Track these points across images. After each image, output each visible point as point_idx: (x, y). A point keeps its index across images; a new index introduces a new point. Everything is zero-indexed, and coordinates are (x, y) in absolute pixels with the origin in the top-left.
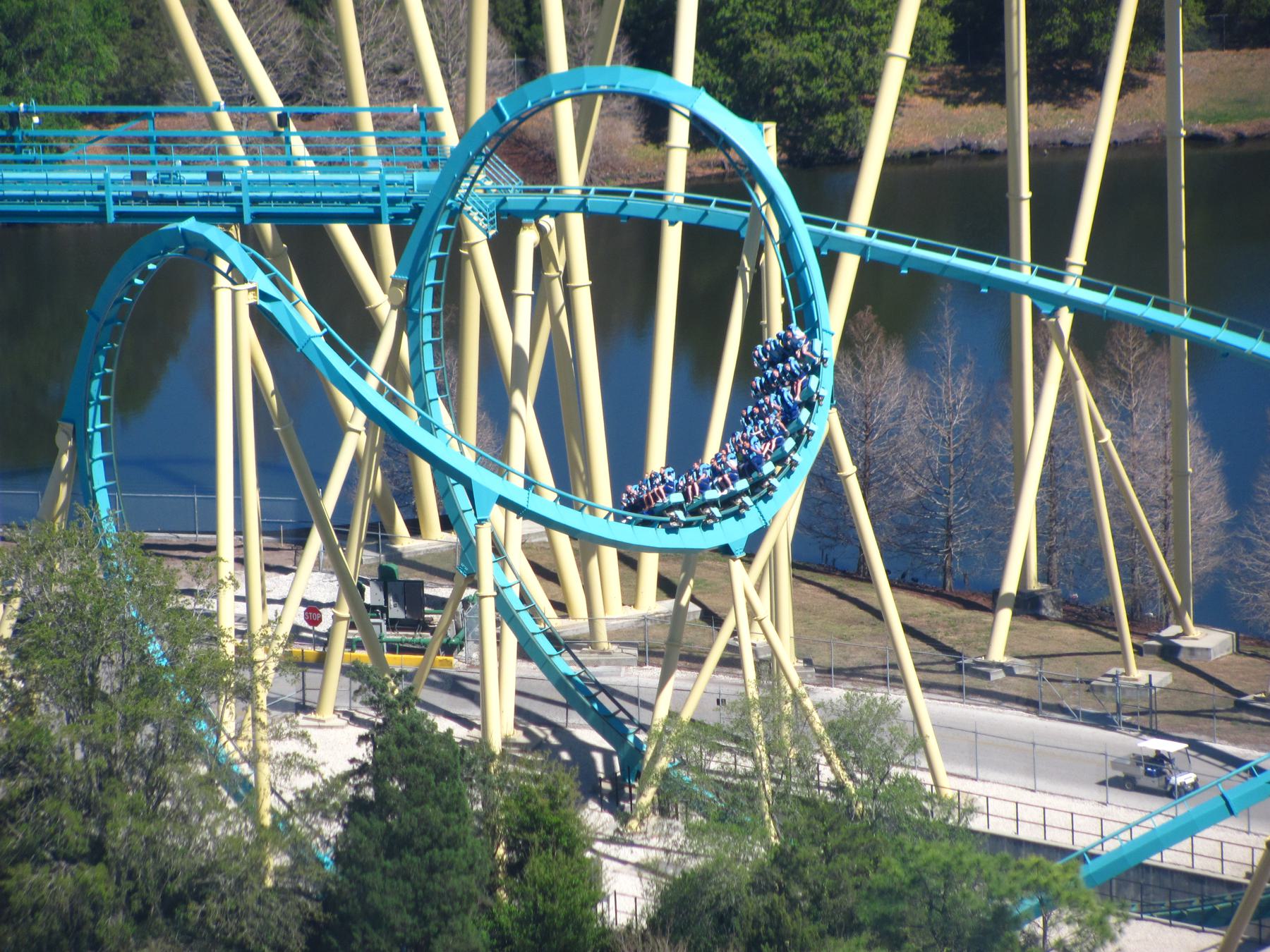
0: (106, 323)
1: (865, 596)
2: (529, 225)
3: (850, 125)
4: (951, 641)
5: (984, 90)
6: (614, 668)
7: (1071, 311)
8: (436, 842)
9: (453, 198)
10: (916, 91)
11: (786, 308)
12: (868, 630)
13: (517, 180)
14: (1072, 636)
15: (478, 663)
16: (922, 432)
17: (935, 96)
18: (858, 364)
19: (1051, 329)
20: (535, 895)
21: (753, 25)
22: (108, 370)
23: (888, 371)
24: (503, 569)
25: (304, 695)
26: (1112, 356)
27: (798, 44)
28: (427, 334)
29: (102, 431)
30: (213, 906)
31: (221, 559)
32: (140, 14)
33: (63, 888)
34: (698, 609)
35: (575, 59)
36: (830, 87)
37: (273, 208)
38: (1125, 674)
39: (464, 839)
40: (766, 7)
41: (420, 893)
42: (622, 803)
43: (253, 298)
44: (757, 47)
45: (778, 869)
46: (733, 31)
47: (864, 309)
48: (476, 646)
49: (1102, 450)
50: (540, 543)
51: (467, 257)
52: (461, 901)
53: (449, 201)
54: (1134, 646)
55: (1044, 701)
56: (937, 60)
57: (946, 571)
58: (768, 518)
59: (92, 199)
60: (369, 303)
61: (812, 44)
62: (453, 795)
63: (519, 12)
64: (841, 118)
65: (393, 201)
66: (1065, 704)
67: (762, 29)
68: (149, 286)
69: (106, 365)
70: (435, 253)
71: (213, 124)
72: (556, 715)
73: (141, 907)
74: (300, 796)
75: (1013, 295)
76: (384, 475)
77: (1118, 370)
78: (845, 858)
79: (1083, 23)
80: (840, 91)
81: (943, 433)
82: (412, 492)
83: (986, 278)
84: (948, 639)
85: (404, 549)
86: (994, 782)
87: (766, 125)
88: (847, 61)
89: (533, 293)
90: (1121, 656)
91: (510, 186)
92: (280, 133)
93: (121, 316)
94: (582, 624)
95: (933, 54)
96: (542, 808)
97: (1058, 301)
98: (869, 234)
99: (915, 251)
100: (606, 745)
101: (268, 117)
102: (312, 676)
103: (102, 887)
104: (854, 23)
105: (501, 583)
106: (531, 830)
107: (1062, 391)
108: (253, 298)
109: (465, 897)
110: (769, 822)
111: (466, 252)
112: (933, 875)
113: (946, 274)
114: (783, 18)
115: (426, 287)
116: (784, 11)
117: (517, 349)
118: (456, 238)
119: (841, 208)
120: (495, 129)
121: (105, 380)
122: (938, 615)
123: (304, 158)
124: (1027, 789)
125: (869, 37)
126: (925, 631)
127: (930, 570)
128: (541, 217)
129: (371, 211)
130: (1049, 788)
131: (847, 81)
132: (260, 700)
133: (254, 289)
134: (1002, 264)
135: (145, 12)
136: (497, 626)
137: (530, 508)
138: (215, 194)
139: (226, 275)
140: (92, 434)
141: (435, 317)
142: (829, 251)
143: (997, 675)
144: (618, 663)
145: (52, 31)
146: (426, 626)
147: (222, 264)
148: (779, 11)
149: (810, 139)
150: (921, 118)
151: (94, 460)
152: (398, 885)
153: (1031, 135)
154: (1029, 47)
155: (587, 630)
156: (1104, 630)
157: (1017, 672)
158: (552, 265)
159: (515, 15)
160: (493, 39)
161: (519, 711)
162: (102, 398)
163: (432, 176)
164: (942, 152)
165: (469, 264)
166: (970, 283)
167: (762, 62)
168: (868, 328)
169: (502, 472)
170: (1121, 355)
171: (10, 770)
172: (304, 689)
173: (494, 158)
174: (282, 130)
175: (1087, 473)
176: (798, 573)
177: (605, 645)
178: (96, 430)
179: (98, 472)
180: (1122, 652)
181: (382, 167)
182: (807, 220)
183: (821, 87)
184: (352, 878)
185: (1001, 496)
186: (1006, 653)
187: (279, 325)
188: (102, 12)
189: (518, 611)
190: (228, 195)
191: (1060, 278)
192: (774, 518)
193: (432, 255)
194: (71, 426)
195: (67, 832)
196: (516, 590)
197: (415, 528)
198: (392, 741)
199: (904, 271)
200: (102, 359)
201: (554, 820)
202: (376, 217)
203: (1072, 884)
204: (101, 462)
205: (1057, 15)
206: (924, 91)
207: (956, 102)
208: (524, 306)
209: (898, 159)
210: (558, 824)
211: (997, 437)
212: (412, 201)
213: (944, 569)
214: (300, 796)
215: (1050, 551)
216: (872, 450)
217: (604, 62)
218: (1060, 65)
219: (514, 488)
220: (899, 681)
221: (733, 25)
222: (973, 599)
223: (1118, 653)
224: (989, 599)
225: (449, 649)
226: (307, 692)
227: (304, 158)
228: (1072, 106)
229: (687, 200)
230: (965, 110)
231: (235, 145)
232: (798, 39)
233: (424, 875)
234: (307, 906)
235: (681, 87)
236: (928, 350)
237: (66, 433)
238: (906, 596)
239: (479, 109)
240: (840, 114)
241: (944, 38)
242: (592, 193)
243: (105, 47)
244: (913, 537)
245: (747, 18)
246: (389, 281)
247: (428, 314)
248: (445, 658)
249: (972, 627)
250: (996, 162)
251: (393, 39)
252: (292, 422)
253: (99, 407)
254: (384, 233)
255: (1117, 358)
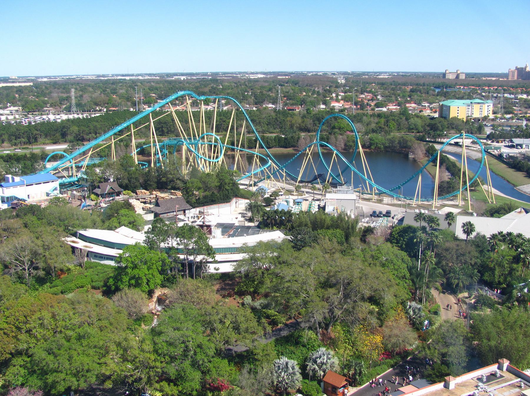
97: (238, 149)
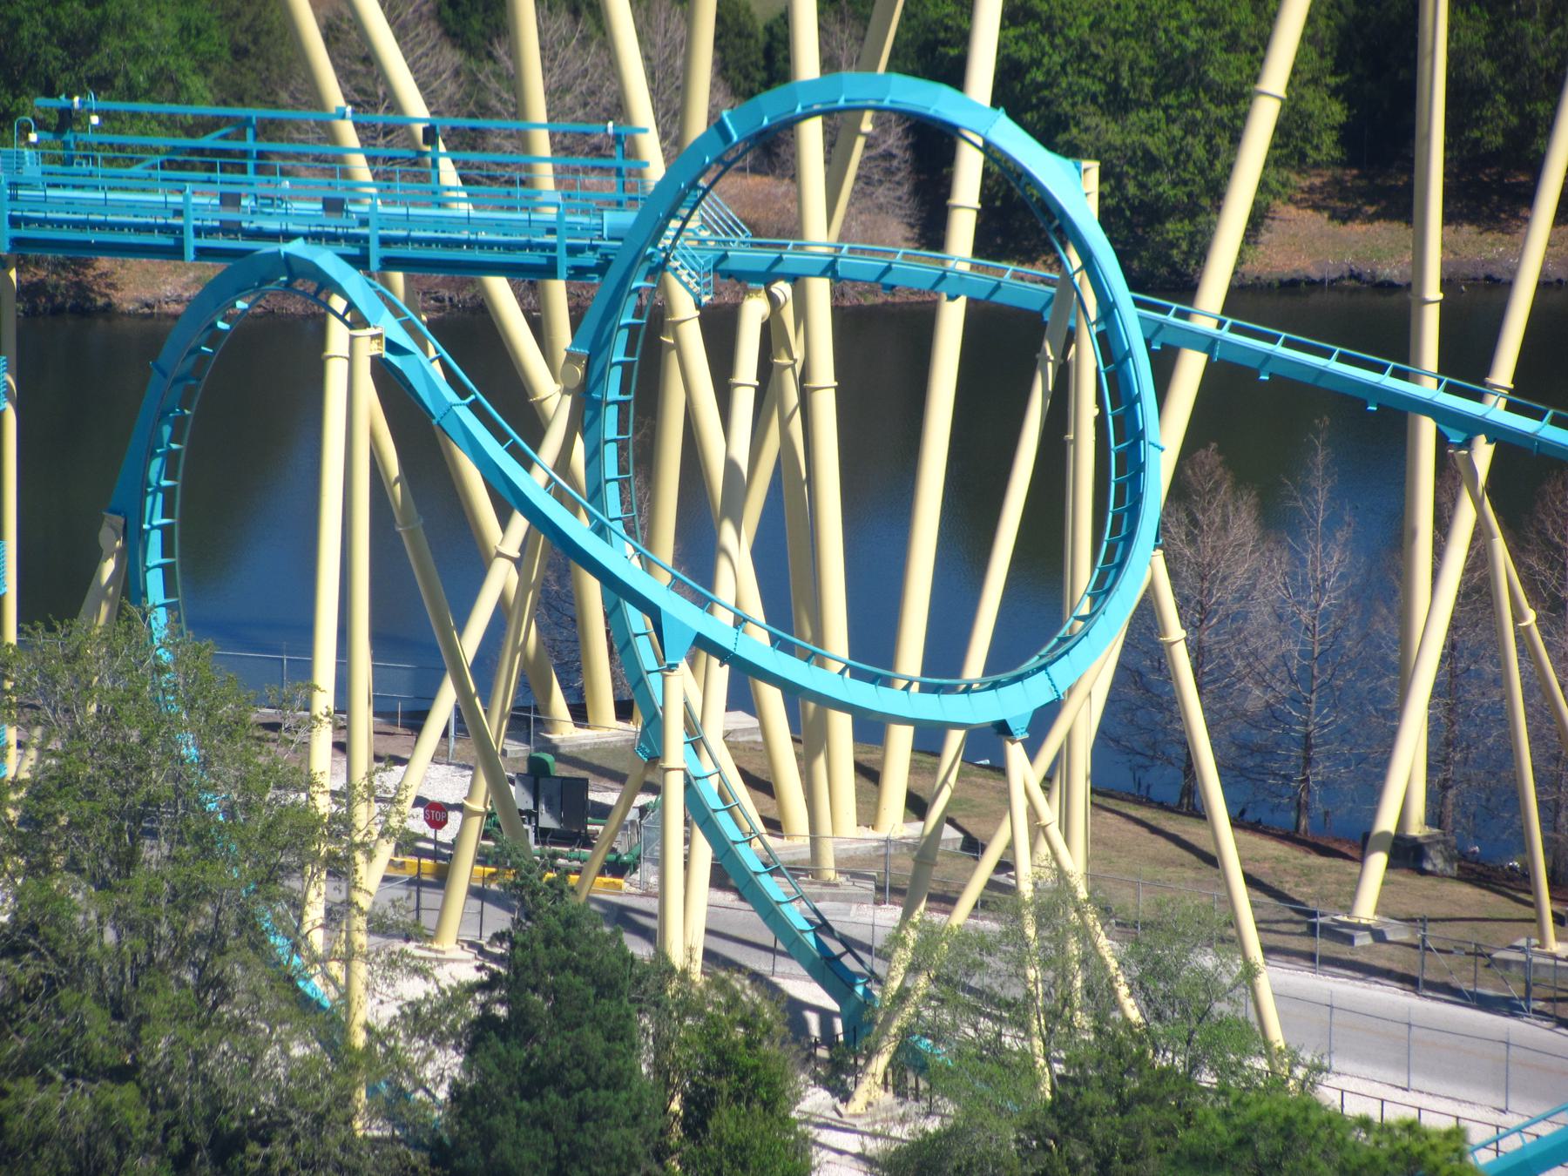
0: (177, 381)
1: (1185, 832)
2: (757, 291)
3: (1199, 237)
4: (1302, 894)
5: (1384, 203)
6: (841, 905)
7: (1489, 442)
8: (593, 1083)
9: (655, 246)
10: (1290, 199)
11: (1100, 422)
12: (1190, 874)
13: (743, 231)
14: (1468, 896)
15: (657, 890)
16: (1280, 617)
17: (1316, 208)
18: (1194, 522)
19: (1461, 466)
20: (720, 1160)
21: (1073, 95)
22: (174, 446)
23: (1236, 532)
24: (697, 751)
25: (418, 917)
26: (1542, 522)
27: (1133, 124)
28: (610, 428)
29: (162, 527)
30: (280, 1148)
31: (316, 688)
32: (244, 40)
33: (78, 1113)
34: (959, 835)
35: (829, 63)
36: (1174, 185)
37: (409, 252)
38: (1539, 946)
39: (629, 1080)
40: (1092, 72)
41: (564, 1147)
42: (844, 1076)
43: (377, 349)
44: (1077, 124)
45: (1054, 1121)
46: (1047, 103)
47: (1206, 446)
48: (656, 869)
49: (1523, 637)
50: (748, 742)
51: (671, 347)
52: (618, 1161)
53: (650, 250)
54: (1554, 914)
55: (1426, 977)
56: (1322, 157)
57: (1300, 807)
58: (1062, 689)
59: (166, 229)
60: (534, 394)
61: (1152, 125)
62: (619, 1017)
63: (755, 65)
64: (1188, 226)
65: (573, 250)
66: (1455, 981)
67: (1084, 101)
68: (235, 333)
69: (172, 440)
70: (627, 319)
71: (331, 136)
72: (759, 962)
73: (182, 1146)
74: (407, 1010)
75: (1411, 415)
76: (538, 627)
77: (1549, 543)
78: (1147, 1111)
79: (1522, 115)
80: (1188, 189)
81: (1305, 617)
82: (579, 670)
83: (1375, 390)
84: (1300, 892)
85: (563, 740)
86: (1352, 1076)
87: (1085, 164)
88: (1200, 152)
89: (757, 383)
90: (1535, 925)
91: (734, 237)
92: (424, 153)
93: (196, 373)
94: (801, 846)
95: (1317, 148)
96: (735, 1046)
97: (1474, 426)
98: (1221, 325)
99: (1279, 349)
100: (831, 1004)
101: (411, 135)
102: (430, 898)
103: (130, 1114)
104: (1211, 100)
105: (693, 772)
106: (719, 1075)
107: (1469, 570)
108: (377, 349)
109: (625, 1158)
110: (1043, 1068)
111: (671, 341)
112: (1267, 1135)
113: (1321, 384)
114: (1114, 88)
115: (612, 365)
116: (1118, 77)
117: (731, 465)
118: (658, 319)
119: (1185, 288)
120: (717, 154)
121: (171, 459)
122: (1286, 861)
123: (455, 189)
124: (1397, 1087)
125: (1231, 119)
126: (1266, 880)
127: (1280, 803)
128: (774, 281)
129: (544, 261)
130: (1428, 1085)
131: (1198, 178)
132: (358, 877)
133: (379, 336)
134: (1397, 374)
135: (250, 38)
136: (685, 844)
137: (737, 652)
138: (332, 230)
139: (341, 318)
140: (147, 532)
141: (622, 405)
142: (1163, 345)
143: (1364, 940)
144: (848, 899)
145: (124, 51)
146: (587, 841)
147: (338, 303)
148: (1111, 77)
149: (1144, 253)
150: (1295, 235)
151: (148, 569)
152: (536, 1136)
153: (1444, 265)
154: (1448, 147)
155: (807, 855)
156: (1513, 893)
157: (1390, 937)
158: (783, 352)
159: (751, 69)
160: (719, 97)
161: (709, 955)
162: (164, 483)
163: (627, 218)
164: (1322, 281)
165: (673, 356)
166: (1349, 400)
167: (1083, 146)
168: (1211, 474)
169: (705, 603)
170: (1554, 522)
171: (14, 951)
172: (418, 909)
173: (711, 197)
174: (428, 148)
175: (1501, 681)
176: (1099, 800)
177: (831, 875)
178: (153, 528)
179: (155, 584)
180: (1537, 920)
181: (561, 202)
182: (1138, 303)
183: (1164, 185)
184: (475, 1123)
185: (1382, 707)
186: (1376, 912)
187: (410, 387)
188: (194, 32)
189: (715, 811)
190: (351, 231)
191: (1478, 397)
192: (1070, 690)
193: (623, 322)
194: (121, 520)
195: (91, 1034)
196: (714, 781)
197: (580, 714)
198: (540, 937)
199: (1265, 377)
200: (167, 431)
201: (751, 1062)
202: (550, 271)
203: (1456, 1155)
204: (159, 571)
205: (1488, 104)
206: (1302, 200)
207: (1344, 217)
208: (744, 401)
209: (1262, 287)
210: (756, 1068)
211: (1380, 626)
212: (600, 251)
213: (1299, 804)
214: (407, 1010)
215: (1445, 786)
216: (1208, 638)
217: (874, 68)
218: (1487, 175)
219: (719, 627)
220: (1231, 941)
221: (1046, 93)
222: (1335, 846)
223: (1532, 921)
224: (1360, 844)
225: (617, 868)
226: (423, 913)
227: (455, 189)
228: (1502, 231)
229: (974, 267)
230: (1357, 229)
231: (361, 170)
232: (1132, 117)
233: (571, 1125)
234: (408, 1156)
235: (977, 107)
236: (1291, 504)
237: (114, 529)
238: (1249, 838)
239: (698, 124)
240: (1187, 222)
241: (1333, 128)
242: (845, 250)
243: (194, 78)
244: (1258, 760)
245: (1064, 85)
246: (561, 356)
247: (613, 403)
248: (612, 880)
249: (1334, 877)
250: (1395, 299)
251: (584, 88)
252: (422, 521)
253: (160, 496)
254: (558, 292)
255: (1549, 525)
